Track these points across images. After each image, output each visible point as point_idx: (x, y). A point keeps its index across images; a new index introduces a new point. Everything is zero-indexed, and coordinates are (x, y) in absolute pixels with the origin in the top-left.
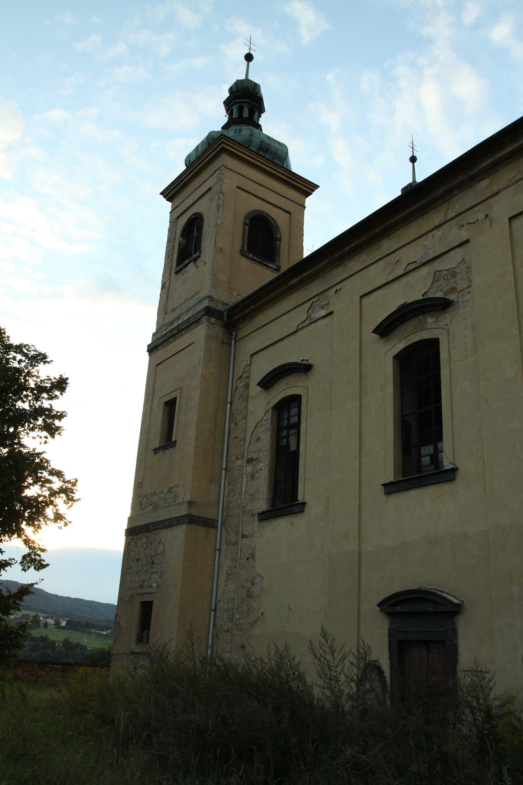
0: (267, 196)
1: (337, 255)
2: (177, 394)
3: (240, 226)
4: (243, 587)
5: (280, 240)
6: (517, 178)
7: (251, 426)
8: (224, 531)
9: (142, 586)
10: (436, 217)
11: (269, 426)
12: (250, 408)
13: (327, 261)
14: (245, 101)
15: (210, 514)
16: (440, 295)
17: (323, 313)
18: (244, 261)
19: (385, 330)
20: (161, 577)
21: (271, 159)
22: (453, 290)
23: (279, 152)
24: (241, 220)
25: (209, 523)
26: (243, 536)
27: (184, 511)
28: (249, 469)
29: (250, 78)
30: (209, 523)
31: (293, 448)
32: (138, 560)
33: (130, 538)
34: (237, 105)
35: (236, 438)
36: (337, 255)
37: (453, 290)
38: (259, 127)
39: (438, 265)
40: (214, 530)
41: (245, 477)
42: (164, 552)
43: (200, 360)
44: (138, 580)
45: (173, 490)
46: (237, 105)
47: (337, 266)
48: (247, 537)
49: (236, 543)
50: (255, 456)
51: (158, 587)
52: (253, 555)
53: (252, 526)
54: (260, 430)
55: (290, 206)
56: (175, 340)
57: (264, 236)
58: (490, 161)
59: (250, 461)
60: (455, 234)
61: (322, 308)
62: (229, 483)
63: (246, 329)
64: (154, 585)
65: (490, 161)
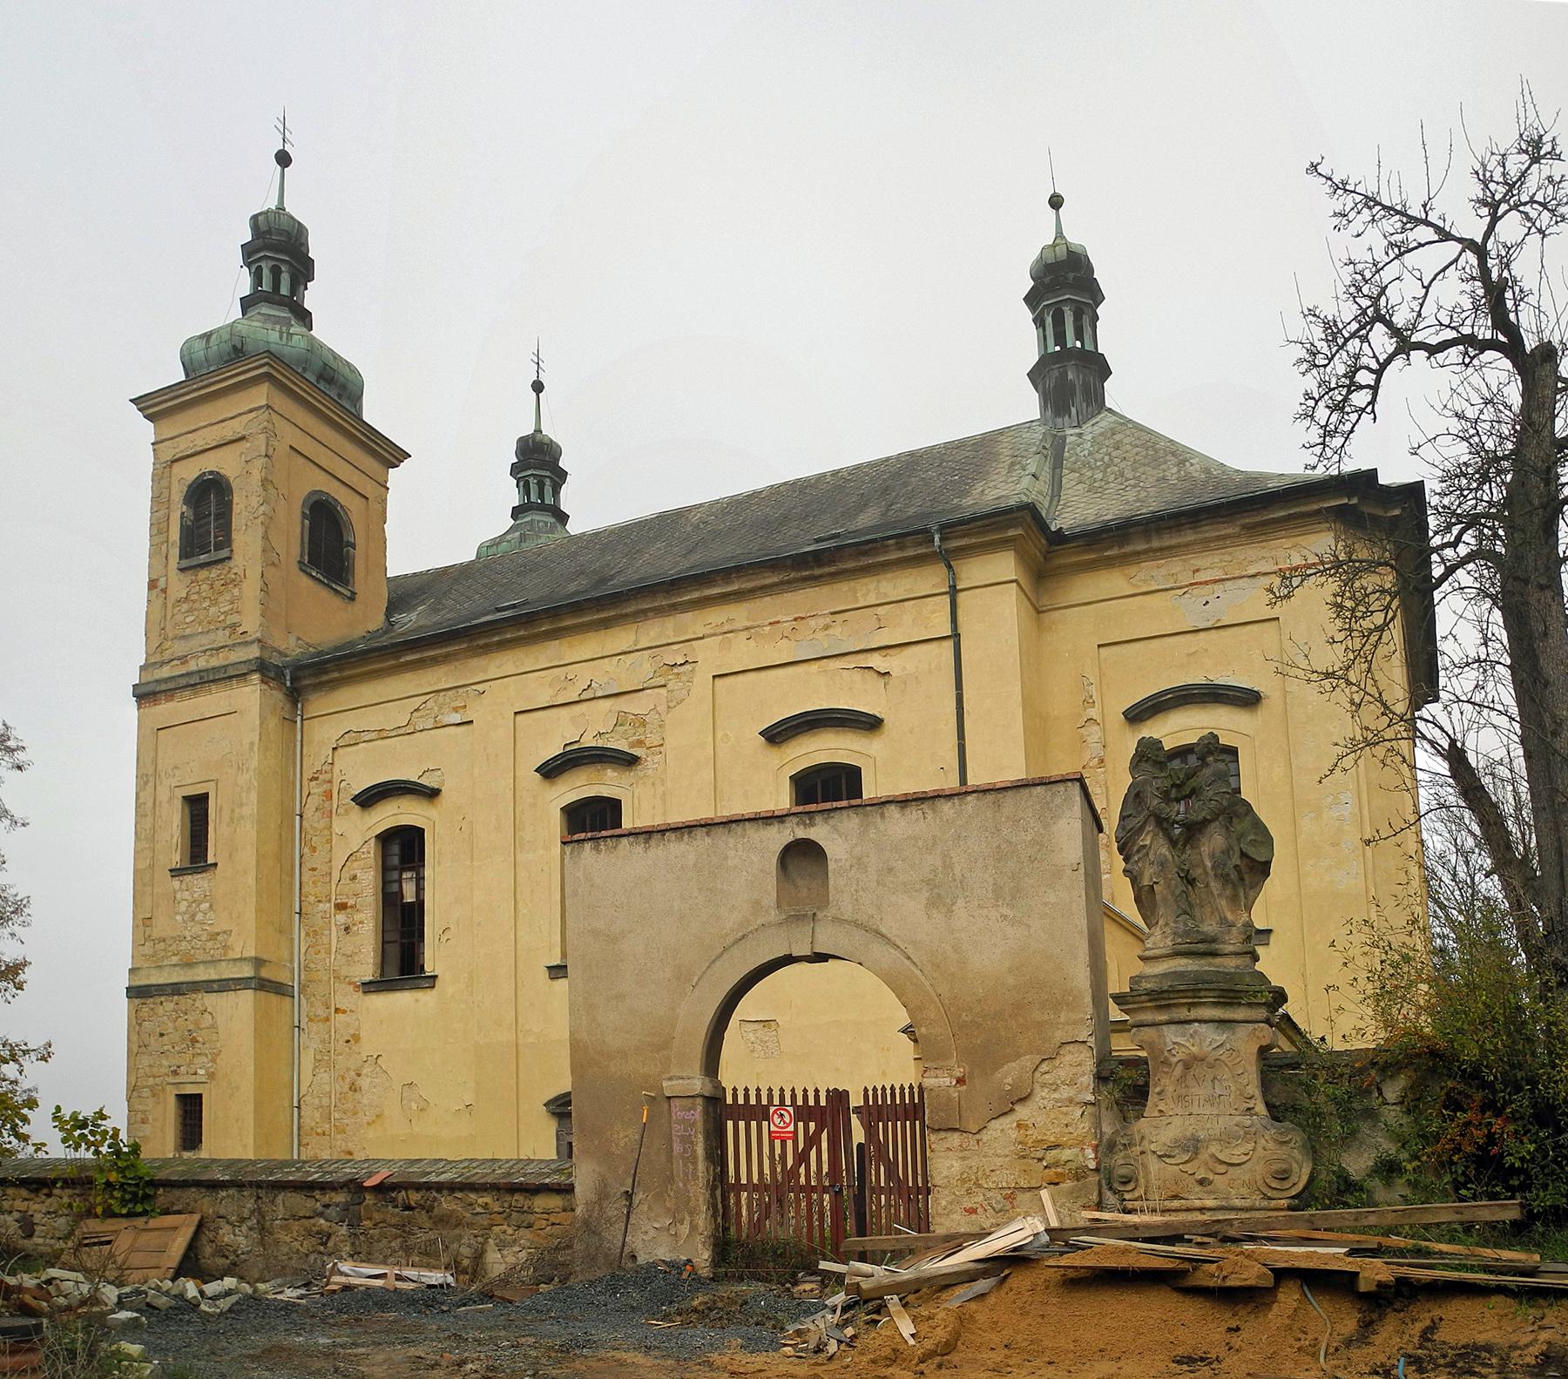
0: (333, 470)
1: (481, 642)
2: (209, 788)
3: (297, 517)
4: (343, 1078)
5: (353, 546)
6: (725, 628)
7: (339, 857)
8: (303, 1001)
9: (175, 1073)
10: (621, 638)
11: (372, 862)
12: (337, 829)
13: (464, 646)
14: (279, 254)
15: (282, 977)
16: (622, 746)
17: (457, 718)
18: (305, 581)
19: (551, 770)
20: (214, 1061)
21: (329, 389)
22: (640, 743)
23: (350, 385)
24: (553, 784)
25: (280, 989)
26: (337, 1010)
27: (247, 971)
28: (341, 918)
29: (290, 208)
30: (280, 989)
31: (409, 897)
32: (162, 1035)
33: (137, 1001)
34: (271, 263)
35: (313, 869)
36: (481, 642)
37: (640, 743)
38: (305, 317)
39: (623, 704)
40: (288, 1000)
41: (334, 934)
42: (213, 1026)
43: (252, 744)
44: (165, 1063)
45: (220, 938)
46: (271, 263)
47: (479, 655)
48: (344, 1012)
49: (327, 1019)
50: (351, 902)
51: (211, 1076)
52: (357, 1038)
53: (347, 998)
54: (355, 864)
55: (368, 488)
56: (196, 695)
57: (330, 543)
58: (696, 595)
59: (341, 907)
60: (641, 669)
61: (456, 710)
62: (307, 934)
63: (318, 704)
64: (201, 1072)
65: (696, 595)
